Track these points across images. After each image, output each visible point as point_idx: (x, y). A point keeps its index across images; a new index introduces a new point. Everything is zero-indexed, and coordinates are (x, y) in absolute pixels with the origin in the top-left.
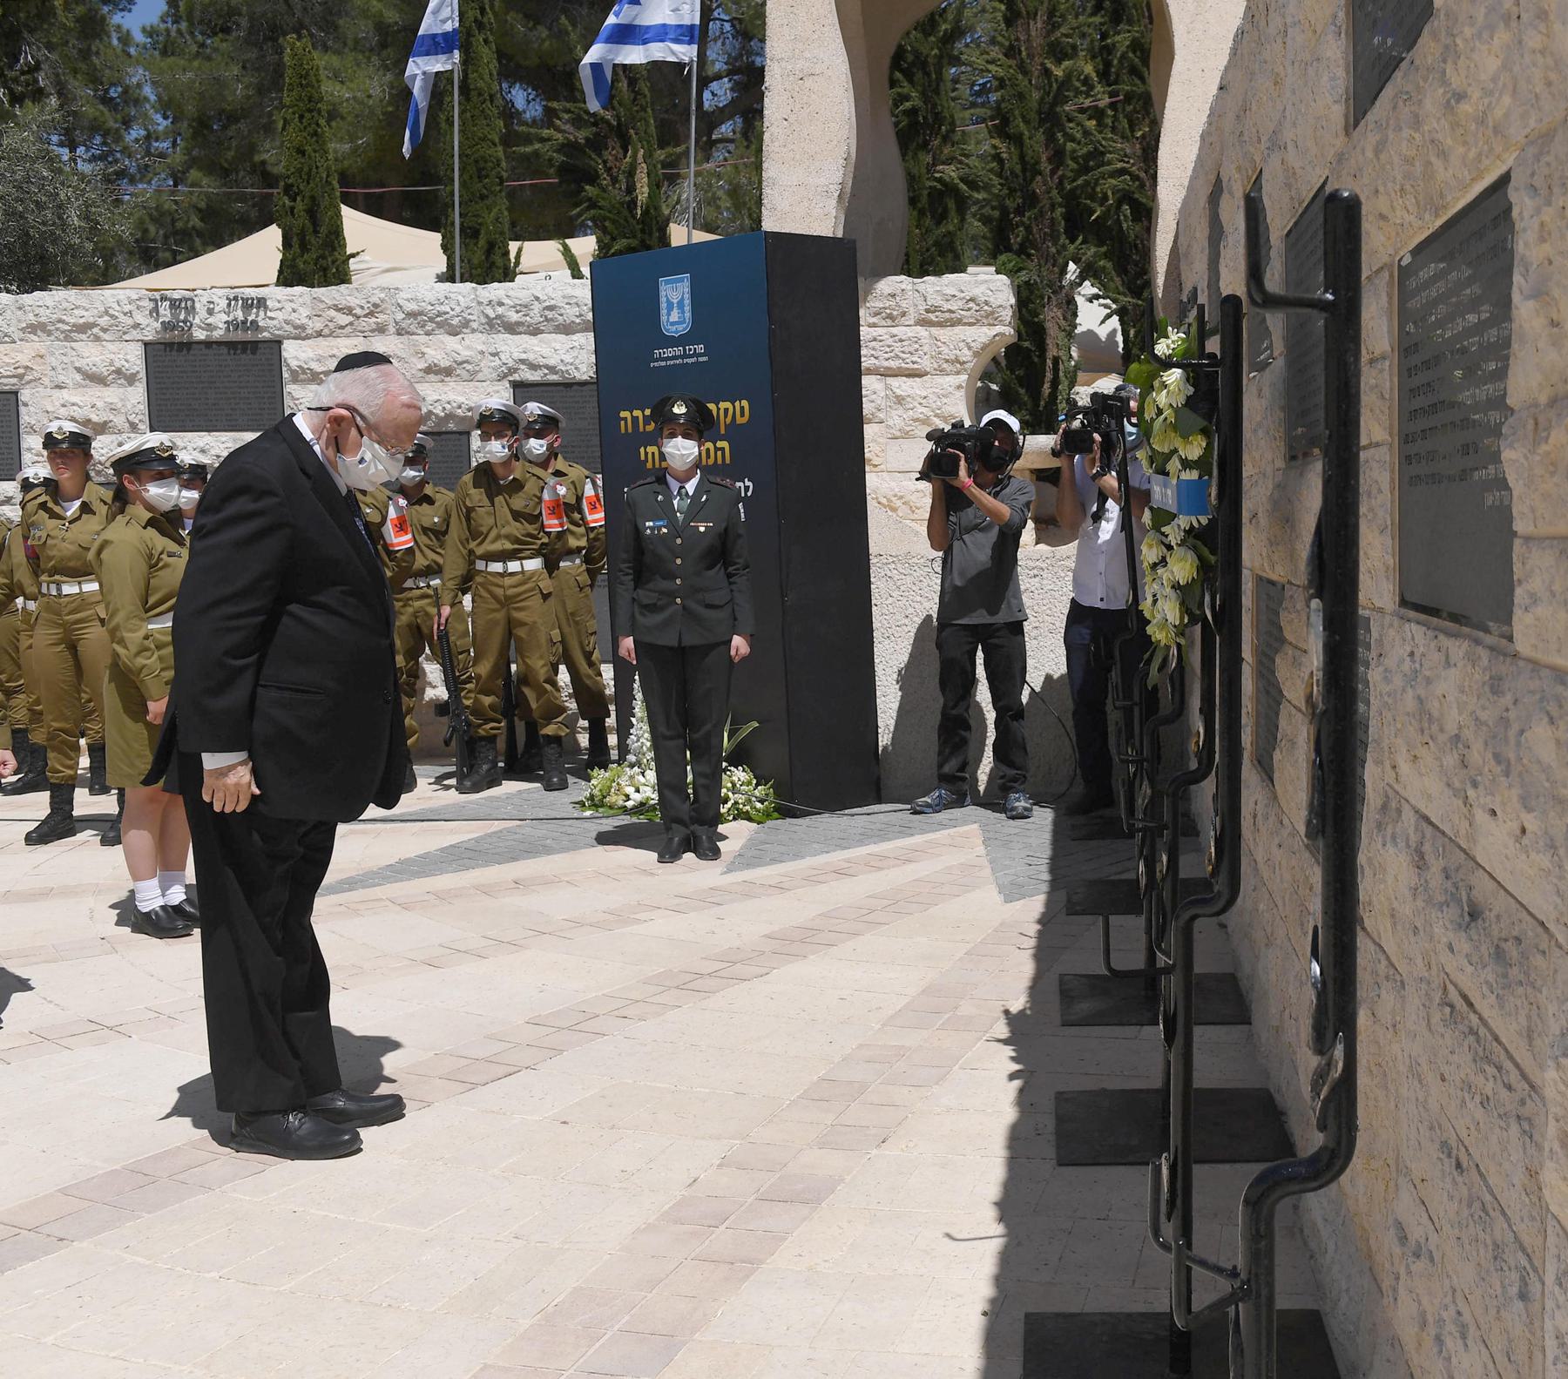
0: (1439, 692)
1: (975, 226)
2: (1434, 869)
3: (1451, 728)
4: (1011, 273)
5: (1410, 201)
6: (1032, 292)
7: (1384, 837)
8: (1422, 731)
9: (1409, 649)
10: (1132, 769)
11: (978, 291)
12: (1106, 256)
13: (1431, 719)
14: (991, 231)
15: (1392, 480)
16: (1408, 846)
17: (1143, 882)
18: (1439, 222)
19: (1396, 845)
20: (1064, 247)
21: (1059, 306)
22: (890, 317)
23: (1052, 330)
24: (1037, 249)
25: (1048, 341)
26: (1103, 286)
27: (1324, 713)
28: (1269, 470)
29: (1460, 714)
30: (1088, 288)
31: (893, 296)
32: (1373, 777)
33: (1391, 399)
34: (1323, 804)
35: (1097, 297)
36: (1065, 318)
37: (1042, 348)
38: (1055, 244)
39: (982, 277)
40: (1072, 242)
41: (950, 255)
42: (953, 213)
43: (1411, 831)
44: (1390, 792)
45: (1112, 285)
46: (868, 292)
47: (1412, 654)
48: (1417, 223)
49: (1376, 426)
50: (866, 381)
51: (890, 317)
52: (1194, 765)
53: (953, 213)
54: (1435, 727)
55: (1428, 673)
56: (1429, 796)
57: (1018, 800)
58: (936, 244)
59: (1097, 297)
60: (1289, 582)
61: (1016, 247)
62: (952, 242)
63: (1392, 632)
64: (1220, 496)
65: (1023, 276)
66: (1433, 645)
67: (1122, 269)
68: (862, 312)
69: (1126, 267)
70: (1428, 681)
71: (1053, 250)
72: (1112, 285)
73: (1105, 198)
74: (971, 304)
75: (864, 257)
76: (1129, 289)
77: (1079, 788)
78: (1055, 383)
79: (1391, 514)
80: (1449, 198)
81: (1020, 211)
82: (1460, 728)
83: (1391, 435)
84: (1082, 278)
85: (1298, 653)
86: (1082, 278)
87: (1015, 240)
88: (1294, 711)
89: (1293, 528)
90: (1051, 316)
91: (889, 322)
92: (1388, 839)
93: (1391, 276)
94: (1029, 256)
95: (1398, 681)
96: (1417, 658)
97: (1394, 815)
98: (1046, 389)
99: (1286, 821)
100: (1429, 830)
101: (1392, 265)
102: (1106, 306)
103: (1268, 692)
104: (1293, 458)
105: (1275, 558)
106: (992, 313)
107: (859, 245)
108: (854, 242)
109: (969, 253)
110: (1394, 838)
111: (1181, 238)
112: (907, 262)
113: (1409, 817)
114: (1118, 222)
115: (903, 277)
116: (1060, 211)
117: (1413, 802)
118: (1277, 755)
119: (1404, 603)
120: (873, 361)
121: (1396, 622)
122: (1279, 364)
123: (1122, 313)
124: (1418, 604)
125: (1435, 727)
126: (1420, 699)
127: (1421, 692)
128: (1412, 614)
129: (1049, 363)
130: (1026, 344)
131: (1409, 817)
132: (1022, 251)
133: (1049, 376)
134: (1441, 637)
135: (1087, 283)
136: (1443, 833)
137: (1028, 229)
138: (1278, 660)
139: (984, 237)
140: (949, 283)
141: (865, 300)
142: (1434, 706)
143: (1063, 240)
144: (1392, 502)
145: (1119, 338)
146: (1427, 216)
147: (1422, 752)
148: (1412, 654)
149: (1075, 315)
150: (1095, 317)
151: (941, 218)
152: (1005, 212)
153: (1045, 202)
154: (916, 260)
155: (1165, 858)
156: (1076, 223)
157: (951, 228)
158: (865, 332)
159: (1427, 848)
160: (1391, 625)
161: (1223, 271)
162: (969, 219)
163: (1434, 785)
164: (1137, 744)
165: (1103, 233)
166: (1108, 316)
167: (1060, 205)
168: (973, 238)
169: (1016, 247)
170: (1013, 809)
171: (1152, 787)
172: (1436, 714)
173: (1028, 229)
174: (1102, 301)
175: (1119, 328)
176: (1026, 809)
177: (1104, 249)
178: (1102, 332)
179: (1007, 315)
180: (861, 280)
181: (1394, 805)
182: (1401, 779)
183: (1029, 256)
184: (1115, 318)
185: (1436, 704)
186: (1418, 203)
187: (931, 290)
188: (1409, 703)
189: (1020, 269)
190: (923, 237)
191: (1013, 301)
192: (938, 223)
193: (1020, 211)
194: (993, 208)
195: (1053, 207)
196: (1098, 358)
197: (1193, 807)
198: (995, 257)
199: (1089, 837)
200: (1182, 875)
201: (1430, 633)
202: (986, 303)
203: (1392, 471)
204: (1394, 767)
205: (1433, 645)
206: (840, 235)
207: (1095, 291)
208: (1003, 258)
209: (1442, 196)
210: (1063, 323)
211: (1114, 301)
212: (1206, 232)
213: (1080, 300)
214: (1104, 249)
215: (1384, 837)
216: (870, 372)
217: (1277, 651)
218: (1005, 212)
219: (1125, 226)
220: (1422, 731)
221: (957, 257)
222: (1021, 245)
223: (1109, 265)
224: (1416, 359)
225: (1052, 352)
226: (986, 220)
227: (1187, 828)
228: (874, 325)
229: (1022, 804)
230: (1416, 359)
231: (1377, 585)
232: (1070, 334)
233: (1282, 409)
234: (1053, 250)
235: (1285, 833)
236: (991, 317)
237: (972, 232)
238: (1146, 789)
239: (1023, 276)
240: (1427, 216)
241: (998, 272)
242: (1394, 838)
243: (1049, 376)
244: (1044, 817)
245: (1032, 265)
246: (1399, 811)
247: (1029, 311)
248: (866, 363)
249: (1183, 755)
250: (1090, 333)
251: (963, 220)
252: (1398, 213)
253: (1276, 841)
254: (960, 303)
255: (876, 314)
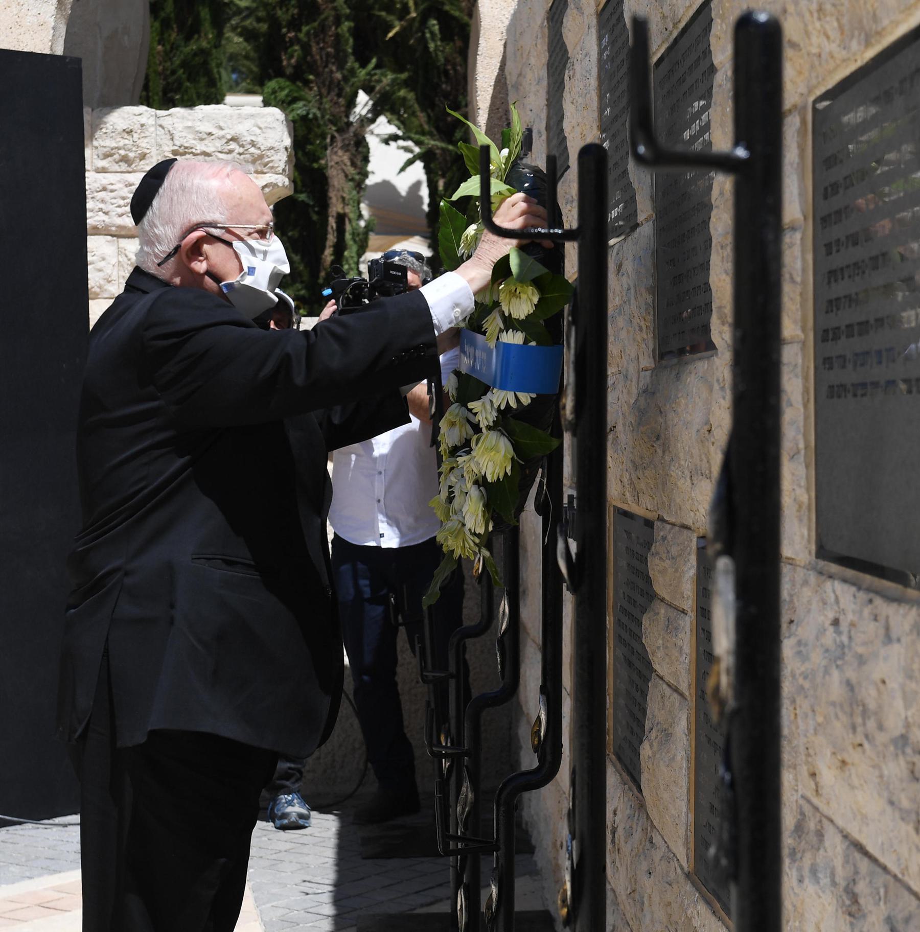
0: (876, 676)
1: (236, 42)
2: (872, 918)
3: (895, 726)
4: (285, 104)
5: (831, 25)
6: (310, 130)
7: (800, 869)
8: (854, 728)
9: (831, 615)
10: (446, 764)
11: (243, 129)
12: (406, 84)
13: (865, 713)
14: (256, 49)
15: (806, 391)
16: (834, 883)
17: (462, 919)
18: (870, 53)
19: (817, 881)
20: (352, 72)
21: (346, 148)
22: (125, 160)
23: (338, 182)
24: (317, 75)
25: (332, 194)
26: (403, 123)
27: (736, 713)
28: (632, 370)
29: (907, 707)
30: (384, 126)
31: (130, 132)
32: (793, 787)
33: (804, 282)
34: (735, 839)
35: (395, 138)
36: (353, 164)
37: (323, 203)
38: (341, 67)
39: (247, 110)
40: (363, 65)
41: (203, 80)
42: (207, 26)
43: (838, 862)
44: (807, 808)
45: (416, 122)
46: (96, 127)
47: (836, 623)
48: (840, 54)
49: (795, 322)
50: (93, 242)
51: (125, 160)
52: (529, 761)
53: (207, 26)
54: (871, 724)
55: (860, 650)
56: (864, 817)
57: (290, 803)
58: (184, 64)
59: (395, 138)
60: (661, 519)
61: (289, 71)
62: (205, 63)
63: (807, 592)
64: (577, 408)
65: (300, 109)
66: (867, 611)
67: (427, 102)
68: (88, 153)
69: (433, 98)
70: (861, 660)
71: (338, 76)
72: (416, 122)
73: (405, 10)
74: (233, 145)
75: (92, 82)
76: (438, 128)
77: (372, 787)
78: (340, 248)
79: (805, 436)
80: (886, 22)
81: (295, 25)
82: (908, 726)
83: (804, 329)
84: (376, 111)
85: (673, 614)
86: (376, 111)
87: (289, 61)
88: (668, 691)
89: (666, 448)
90: (335, 160)
91: (124, 166)
92: (806, 872)
93: (804, 122)
94: (307, 83)
95: (817, 658)
96: (844, 626)
97: (815, 840)
98: (328, 255)
99: (657, 839)
100: (864, 865)
101: (804, 108)
102: (407, 149)
103: (630, 664)
104: (662, 356)
105: (642, 485)
106: (261, 157)
107: (84, 64)
108: (79, 61)
109: (226, 76)
110: (814, 871)
111: (508, 63)
112: (146, 87)
113: (834, 846)
114: (423, 41)
115: (143, 108)
116: (347, 25)
117: (840, 822)
118: (646, 750)
119: (822, 552)
120: (101, 217)
121: (813, 577)
122: (646, 230)
123: (427, 158)
124: (853, 555)
125: (871, 724)
126: (850, 685)
127: (851, 674)
128: (834, 568)
129: (332, 222)
130: (302, 197)
131: (834, 846)
132: (298, 76)
133: (331, 238)
134: (878, 601)
135: (382, 119)
136: (885, 869)
137: (306, 48)
138: (645, 622)
139: (247, 57)
140: (204, 115)
141: (92, 137)
142: (869, 695)
143: (351, 62)
144: (806, 418)
145: (424, 192)
146: (854, 45)
147: (853, 756)
148: (836, 623)
149: (366, 160)
150: (393, 163)
151: (191, 31)
152: (275, 24)
153: (328, 13)
154: (158, 85)
155: (494, 890)
156: (368, 43)
157: (204, 44)
158: (92, 180)
159: (861, 887)
160: (806, 582)
161: (569, 108)
162: (228, 34)
163: (870, 801)
164: (453, 731)
165: (401, 55)
166: (410, 162)
167: (348, 18)
168: (232, 57)
169: (289, 71)
170: (285, 816)
171: (475, 788)
172: (872, 705)
173: (306, 48)
174: (401, 143)
175: (423, 177)
176: (301, 816)
177: (404, 76)
178: (403, 184)
179: (281, 159)
180: (88, 115)
181: (812, 825)
182: (824, 791)
183: (307, 83)
184: (419, 165)
185: (873, 692)
186: (841, 27)
187: (179, 126)
188: (836, 690)
189: (295, 100)
190: (168, 55)
191: (288, 142)
192: (188, 39)
193: (295, 25)
194: (259, 20)
195: (338, 22)
196: (395, 215)
197: (525, 814)
198: (262, 84)
199: (387, 853)
200: (518, 908)
201: (862, 596)
202: (253, 144)
203: (806, 379)
204: (813, 775)
205: (867, 611)
206: (59, 51)
207: (392, 129)
208: (272, 84)
209: (875, 18)
210: (351, 170)
211: (418, 143)
212: (544, 58)
213: (373, 141)
214: (404, 76)
215: (800, 869)
216: (97, 231)
217: (644, 611)
218: (275, 24)
219: (432, 46)
220: (854, 728)
221: (212, 82)
222: (297, 67)
223: (411, 96)
224: (837, 232)
225: (336, 207)
226: (249, 35)
227: (518, 843)
228: (104, 170)
229: (295, 808)
230: (837, 232)
231: (796, 538)
232: (359, 185)
233: (650, 290)
234: (338, 76)
235: (657, 855)
236: (260, 162)
237: (231, 49)
238: (467, 790)
239: (300, 109)
240: (854, 45)
241: (266, 103)
242: (814, 871)
243: (331, 238)
244: (325, 827)
245: (311, 94)
246: (820, 835)
247: (306, 154)
248: (93, 219)
249: (511, 746)
250: (386, 186)
251: (220, 35)
252: (814, 39)
253: (644, 866)
254: (218, 144)
255: (106, 156)
